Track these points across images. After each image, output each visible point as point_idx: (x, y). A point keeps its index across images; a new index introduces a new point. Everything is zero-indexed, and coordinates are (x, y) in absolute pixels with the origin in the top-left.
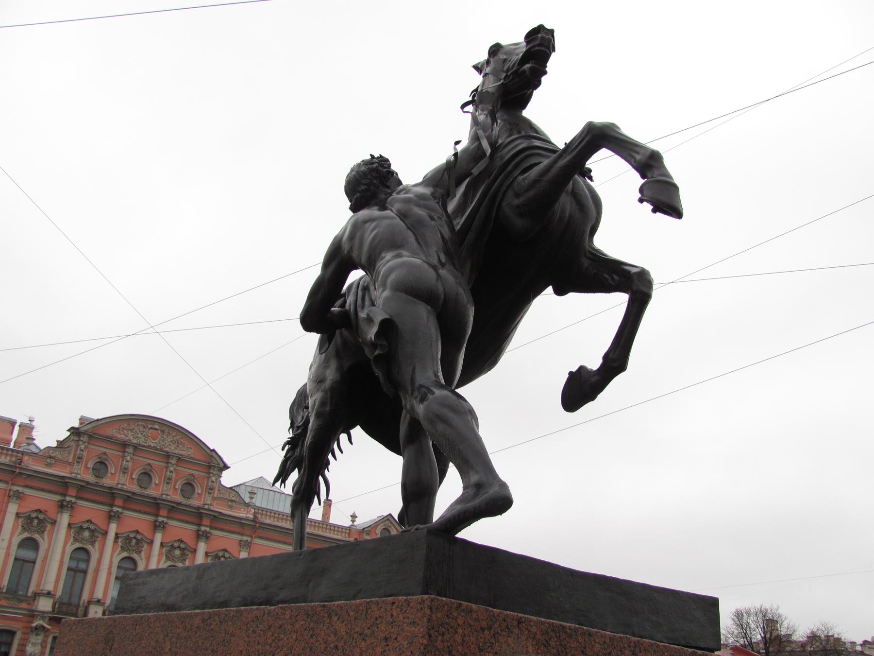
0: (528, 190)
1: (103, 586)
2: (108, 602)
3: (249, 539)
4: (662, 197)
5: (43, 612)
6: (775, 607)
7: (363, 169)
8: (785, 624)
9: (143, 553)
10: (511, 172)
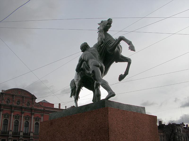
0: (111, 47)
1: (32, 128)
2: (13, 130)
3: (43, 114)
4: (132, 48)
5: (10, 135)
6: (161, 118)
7: (83, 45)
8: (163, 122)
9: (30, 120)
10: (108, 44)
